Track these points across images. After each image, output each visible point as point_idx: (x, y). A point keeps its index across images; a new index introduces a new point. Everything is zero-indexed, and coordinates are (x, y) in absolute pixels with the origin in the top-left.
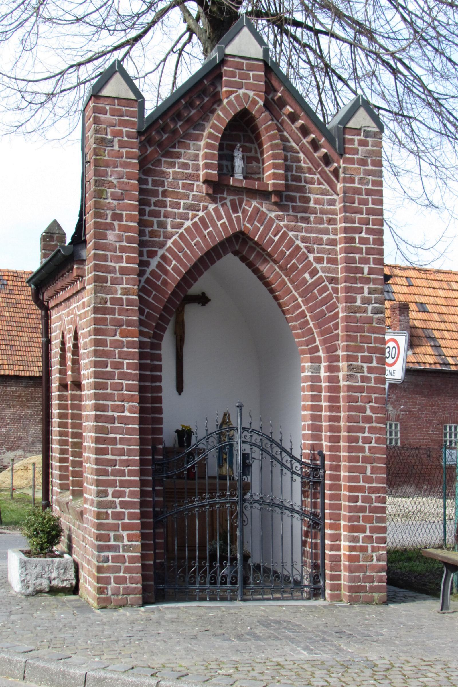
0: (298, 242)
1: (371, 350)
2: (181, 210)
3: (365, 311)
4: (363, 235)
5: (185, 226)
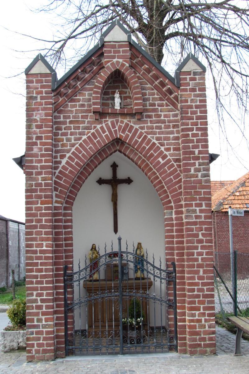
0: (154, 141)
2: (80, 130)
3: (197, 177)
4: (195, 132)
5: (83, 139)
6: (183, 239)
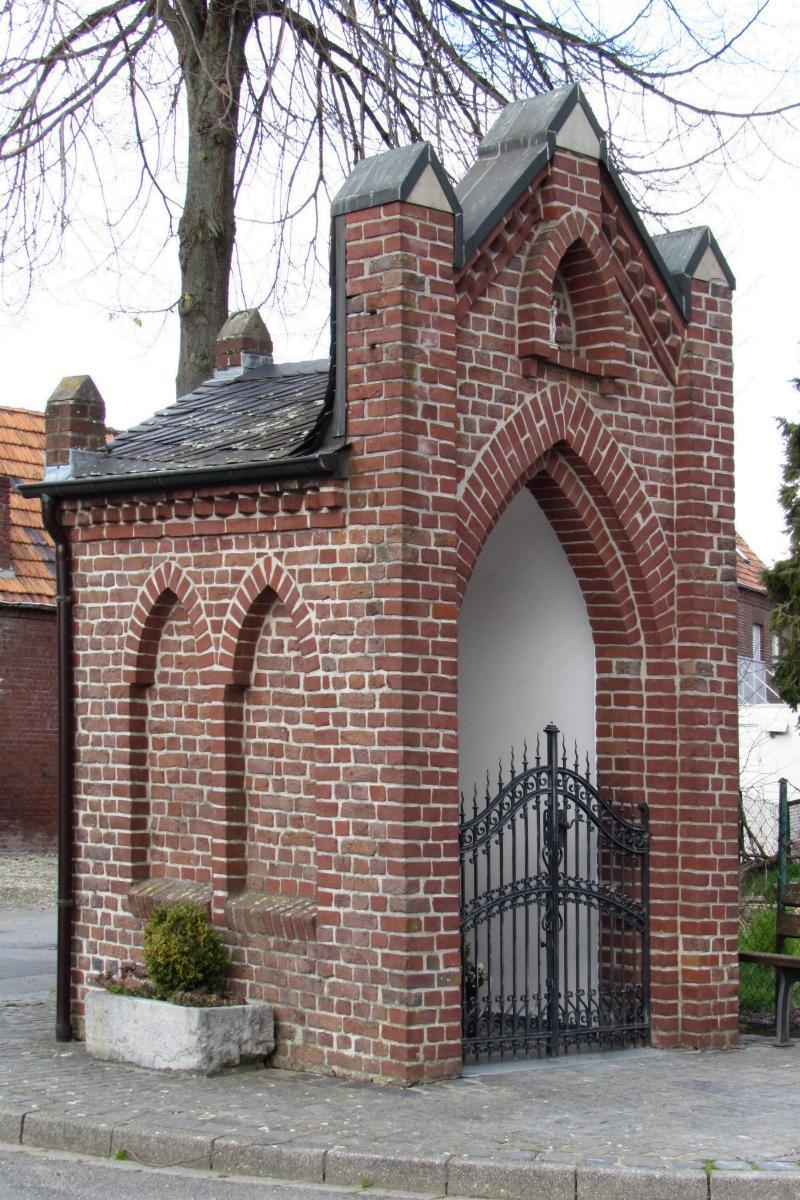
1: (724, 639)
5: (498, 429)
6: (673, 743)
